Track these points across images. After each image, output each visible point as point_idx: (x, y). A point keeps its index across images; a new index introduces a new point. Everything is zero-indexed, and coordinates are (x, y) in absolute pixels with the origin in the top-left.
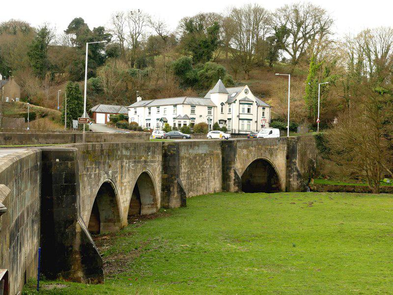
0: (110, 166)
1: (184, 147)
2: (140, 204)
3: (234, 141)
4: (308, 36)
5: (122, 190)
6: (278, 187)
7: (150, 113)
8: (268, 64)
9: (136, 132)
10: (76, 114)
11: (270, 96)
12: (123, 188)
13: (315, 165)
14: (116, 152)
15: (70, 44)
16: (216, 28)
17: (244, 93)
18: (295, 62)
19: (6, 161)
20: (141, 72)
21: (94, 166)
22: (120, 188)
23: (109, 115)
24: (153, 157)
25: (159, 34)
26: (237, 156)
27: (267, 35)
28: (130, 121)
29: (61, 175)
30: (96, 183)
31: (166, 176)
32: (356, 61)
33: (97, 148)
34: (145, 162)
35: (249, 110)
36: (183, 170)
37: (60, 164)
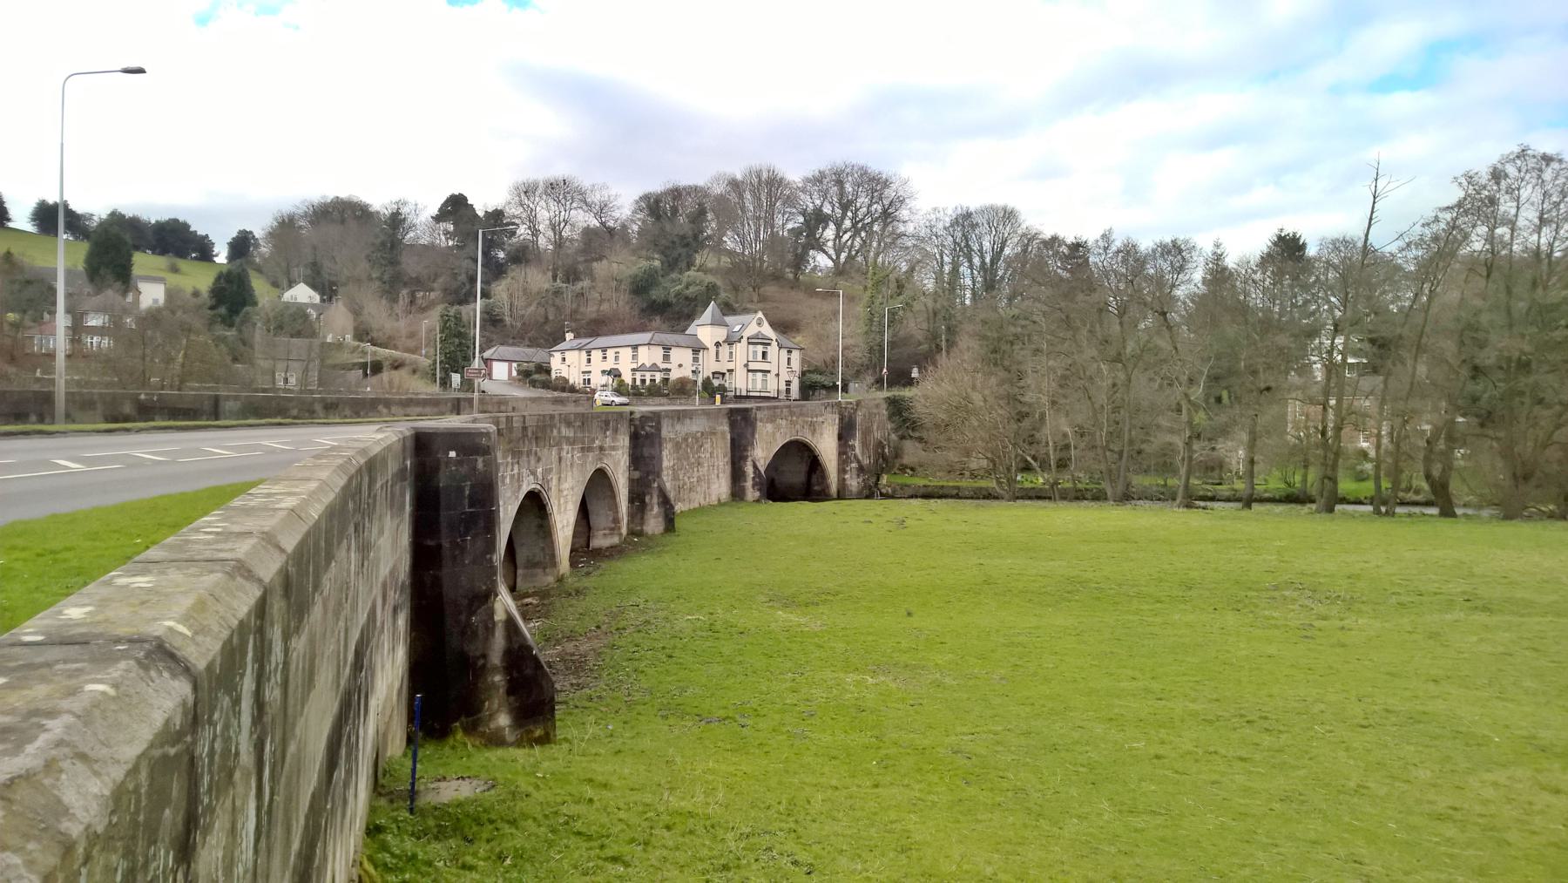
0: (539, 460)
1: (666, 420)
2: (589, 528)
3: (752, 409)
4: (860, 225)
5: (559, 504)
6: (824, 490)
7: (589, 361)
8: (791, 276)
9: (565, 395)
10: (456, 361)
11: (798, 330)
12: (562, 501)
13: (886, 450)
14: (549, 431)
15: (443, 242)
16: (701, 212)
17: (755, 324)
18: (840, 271)
19: (324, 475)
20: (570, 290)
21: (509, 459)
22: (556, 502)
23: (515, 365)
24: (614, 439)
25: (601, 223)
26: (757, 436)
27: (790, 226)
28: (553, 375)
29: (460, 490)
30: (513, 493)
31: (637, 475)
32: (947, 269)
33: (515, 425)
34: (601, 448)
35: (764, 354)
36: (665, 464)
37: (459, 462)
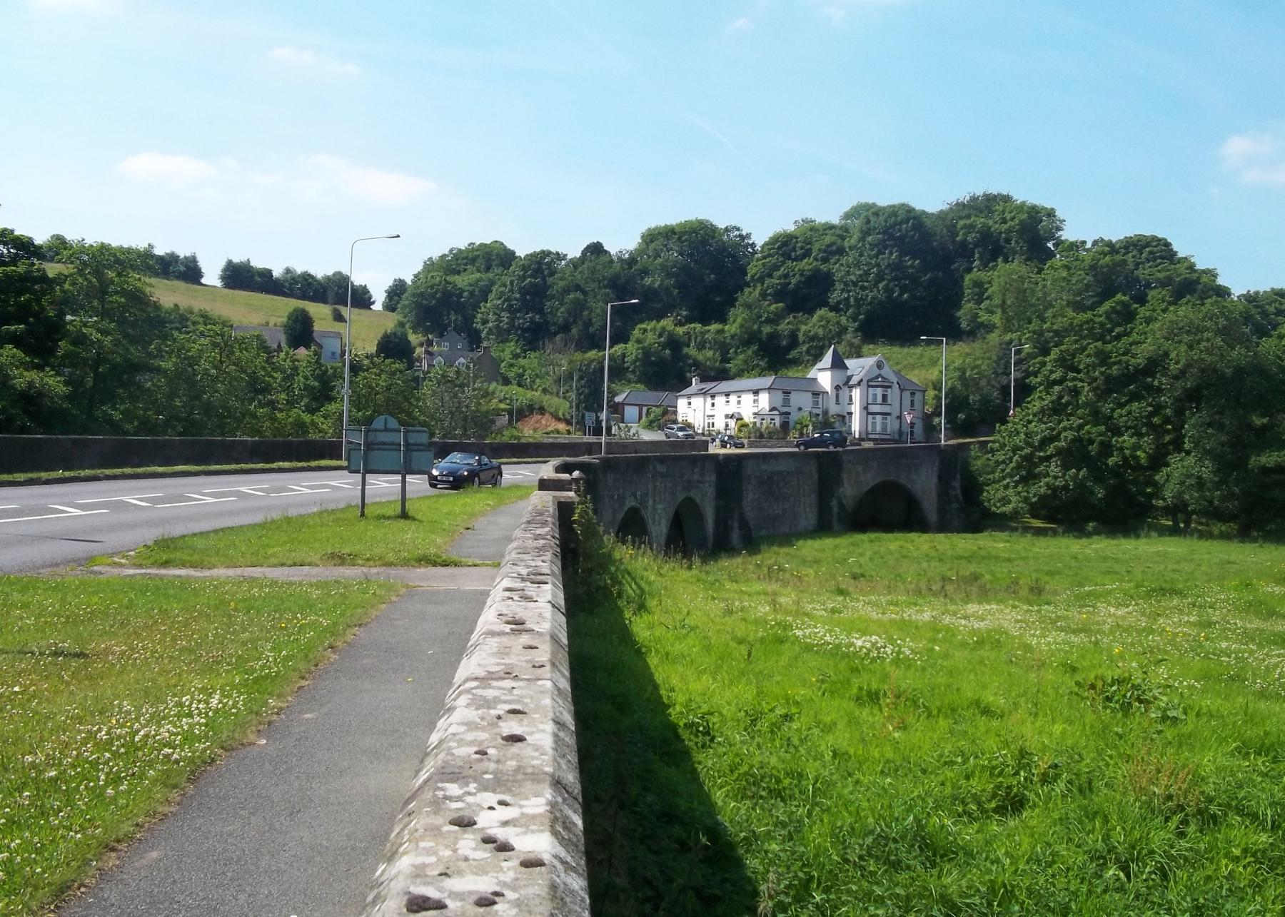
12: (657, 517)
23: (645, 409)
35: (884, 397)
